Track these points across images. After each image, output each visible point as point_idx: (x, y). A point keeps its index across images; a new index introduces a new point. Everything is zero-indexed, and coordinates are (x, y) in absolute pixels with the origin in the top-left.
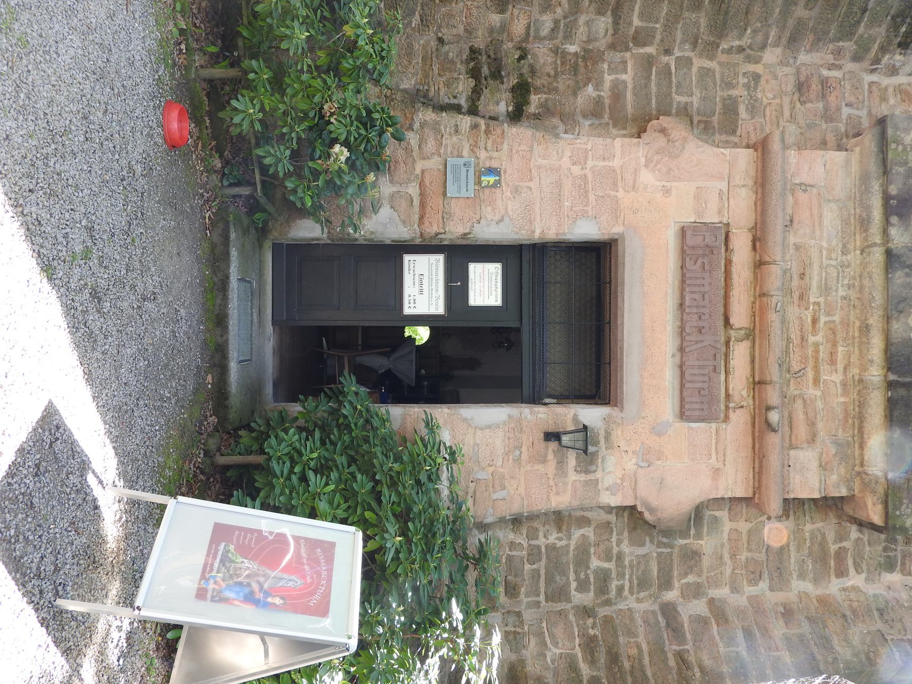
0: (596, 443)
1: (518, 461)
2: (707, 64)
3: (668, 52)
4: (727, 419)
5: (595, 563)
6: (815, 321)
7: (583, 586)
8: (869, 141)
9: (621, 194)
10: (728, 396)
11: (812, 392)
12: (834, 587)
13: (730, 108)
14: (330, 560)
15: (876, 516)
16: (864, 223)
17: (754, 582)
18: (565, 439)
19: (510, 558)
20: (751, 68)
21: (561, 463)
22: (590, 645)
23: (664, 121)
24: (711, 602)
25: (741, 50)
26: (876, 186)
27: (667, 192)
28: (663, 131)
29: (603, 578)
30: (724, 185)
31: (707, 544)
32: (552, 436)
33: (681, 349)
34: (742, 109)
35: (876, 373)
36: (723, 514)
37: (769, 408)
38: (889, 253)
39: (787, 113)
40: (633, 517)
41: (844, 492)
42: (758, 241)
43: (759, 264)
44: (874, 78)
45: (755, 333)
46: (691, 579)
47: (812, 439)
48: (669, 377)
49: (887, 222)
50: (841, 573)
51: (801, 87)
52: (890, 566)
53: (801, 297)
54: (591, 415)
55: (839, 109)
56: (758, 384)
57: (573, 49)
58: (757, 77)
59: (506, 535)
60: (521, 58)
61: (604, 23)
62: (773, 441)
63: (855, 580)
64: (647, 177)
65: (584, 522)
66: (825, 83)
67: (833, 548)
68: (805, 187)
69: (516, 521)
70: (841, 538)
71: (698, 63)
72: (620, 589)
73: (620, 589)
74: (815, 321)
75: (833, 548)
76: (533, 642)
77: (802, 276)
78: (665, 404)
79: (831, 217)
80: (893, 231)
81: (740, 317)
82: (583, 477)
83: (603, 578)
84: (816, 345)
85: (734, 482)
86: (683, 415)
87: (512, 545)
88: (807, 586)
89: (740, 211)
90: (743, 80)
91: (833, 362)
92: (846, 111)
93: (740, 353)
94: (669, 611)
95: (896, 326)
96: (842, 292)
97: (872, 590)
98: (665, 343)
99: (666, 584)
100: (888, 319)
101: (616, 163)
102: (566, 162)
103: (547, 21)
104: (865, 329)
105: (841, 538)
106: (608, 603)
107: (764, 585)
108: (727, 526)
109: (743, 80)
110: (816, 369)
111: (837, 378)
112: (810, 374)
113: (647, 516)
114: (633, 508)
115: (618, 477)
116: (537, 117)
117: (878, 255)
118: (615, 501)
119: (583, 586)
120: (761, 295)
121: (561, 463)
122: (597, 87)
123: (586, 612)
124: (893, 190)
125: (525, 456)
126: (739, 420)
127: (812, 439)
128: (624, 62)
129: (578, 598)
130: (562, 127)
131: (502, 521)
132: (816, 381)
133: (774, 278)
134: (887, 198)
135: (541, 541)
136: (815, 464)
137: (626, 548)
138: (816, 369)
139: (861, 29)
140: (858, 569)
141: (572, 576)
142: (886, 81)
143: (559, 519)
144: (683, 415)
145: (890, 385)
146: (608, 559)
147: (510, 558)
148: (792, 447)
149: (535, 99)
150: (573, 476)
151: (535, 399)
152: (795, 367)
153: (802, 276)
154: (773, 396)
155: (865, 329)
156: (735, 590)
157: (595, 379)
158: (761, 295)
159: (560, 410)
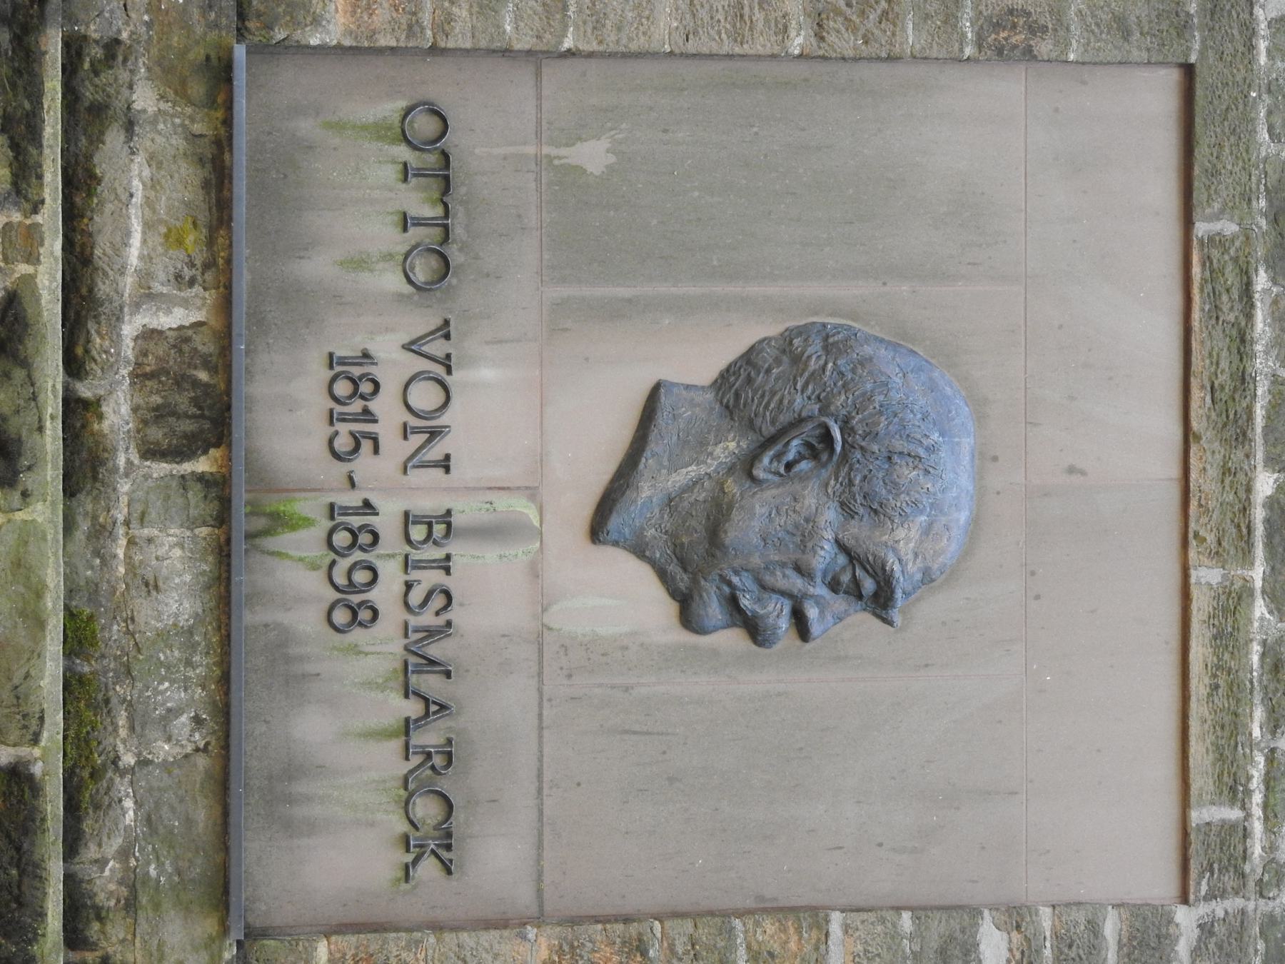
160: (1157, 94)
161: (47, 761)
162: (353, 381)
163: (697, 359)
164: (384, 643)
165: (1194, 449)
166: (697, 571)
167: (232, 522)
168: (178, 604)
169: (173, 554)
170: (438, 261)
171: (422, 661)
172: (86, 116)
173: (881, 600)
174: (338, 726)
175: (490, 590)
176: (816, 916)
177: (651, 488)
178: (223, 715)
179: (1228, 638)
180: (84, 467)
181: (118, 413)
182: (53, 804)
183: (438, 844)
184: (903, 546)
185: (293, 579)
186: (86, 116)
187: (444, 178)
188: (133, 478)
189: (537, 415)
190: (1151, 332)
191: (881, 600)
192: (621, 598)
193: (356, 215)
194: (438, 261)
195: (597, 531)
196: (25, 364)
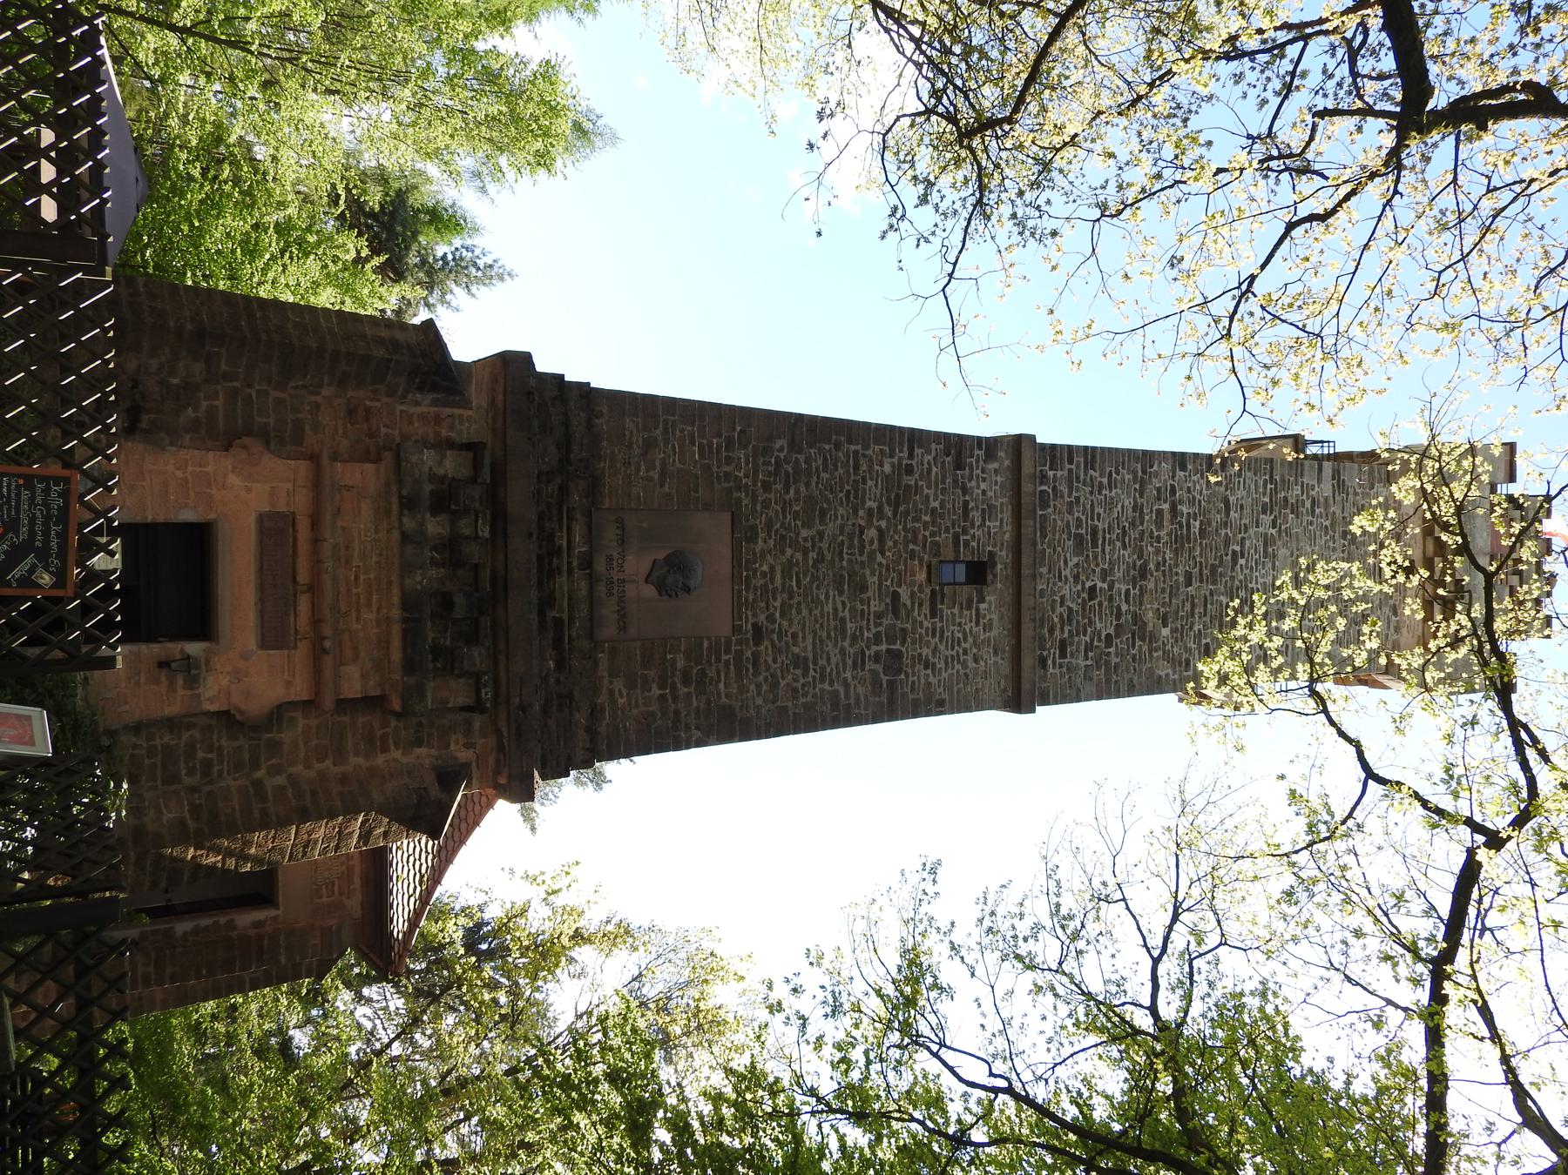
0: (198, 667)
1: (137, 683)
2: (282, 395)
3: (250, 386)
4: (296, 647)
5: (201, 755)
6: (357, 578)
7: (191, 772)
8: (388, 457)
9: (214, 491)
10: (296, 631)
11: (355, 626)
12: (380, 760)
13: (299, 427)
14: (31, 725)
15: (397, 707)
16: (388, 513)
17: (321, 760)
18: (174, 665)
19: (132, 756)
20: (313, 398)
21: (172, 683)
22: (196, 811)
23: (246, 440)
24: (290, 777)
25: (304, 387)
26: (394, 489)
27: (248, 490)
28: (245, 447)
29: (207, 765)
30: (290, 486)
31: (286, 736)
32: (163, 664)
33: (261, 600)
34: (307, 428)
35: (396, 613)
36: (298, 714)
37: (323, 638)
38: (403, 534)
39: (341, 432)
40: (228, 719)
41: (378, 693)
42: (315, 522)
43: (316, 541)
44: (403, 407)
45: (314, 588)
46: (274, 761)
47: (356, 658)
48: (252, 617)
49: (401, 515)
50: (385, 750)
51: (351, 413)
52: (419, 743)
53: (347, 562)
54: (194, 648)
55: (378, 429)
56: (316, 622)
57: (175, 381)
58: (318, 406)
59: (125, 739)
60: (134, 387)
61: (198, 368)
62: (328, 660)
63: (395, 754)
64: (233, 479)
65: (190, 726)
66: (368, 410)
67: (379, 733)
68: (348, 488)
69: (137, 728)
70: (384, 725)
71: (274, 394)
72: (220, 772)
73: (220, 772)
74: (357, 578)
75: (379, 733)
76: (152, 812)
77: (347, 548)
78: (251, 641)
79: (366, 509)
80: (405, 520)
81: (303, 577)
82: (189, 692)
83: (207, 765)
84: (358, 594)
85: (300, 690)
86: (264, 645)
87: (135, 746)
88: (360, 761)
89: (302, 502)
90: (307, 408)
91: (369, 605)
92: (384, 430)
93: (304, 603)
94: (258, 784)
95: (407, 581)
96: (375, 559)
97: (405, 760)
98: (249, 596)
99: (255, 766)
100: (402, 577)
101: (209, 469)
102: (171, 468)
103: (154, 364)
104: (390, 583)
105: (384, 725)
106: (211, 782)
107: (328, 762)
108: (301, 723)
109: (307, 408)
110: (358, 610)
111: (372, 616)
112: (354, 614)
113: (238, 717)
114: (228, 712)
115: (214, 691)
116: (147, 431)
117: (396, 535)
118: (213, 708)
119: (191, 772)
120: (317, 561)
121: (172, 683)
122: (196, 409)
123: (194, 789)
124: (404, 493)
125: (143, 680)
126: (304, 647)
127: (356, 658)
128: (217, 392)
129: (188, 781)
130: (167, 441)
131: (126, 727)
132: (358, 619)
133: (326, 549)
134: (401, 497)
135: (158, 742)
136: (357, 675)
137: (224, 743)
138: (358, 610)
139: (389, 378)
140: (397, 747)
141: (182, 765)
142: (412, 410)
143: (171, 724)
144: (264, 645)
145: (405, 620)
146: (211, 751)
147: (132, 756)
148: (342, 664)
149: (145, 418)
150: (181, 692)
151: (150, 639)
152: (344, 609)
153: (347, 548)
154: (327, 630)
155: (390, 583)
156: (308, 766)
157: (201, 624)
158: (317, 561)
159: (170, 645)
160: (727, 517)
161: (565, 616)
162: (610, 558)
163: (661, 555)
164: (615, 598)
165: (1287, 242)
166: (661, 587)
167: (592, 580)
168: (584, 593)
169: (583, 584)
170: (622, 541)
171: (621, 601)
172: (570, 519)
173: (688, 592)
174: (608, 611)
175: (631, 590)
176: (679, 639)
177: (655, 574)
178: (591, 609)
179: (740, 596)
180: (570, 572)
181: (575, 564)
182: (303, 527)
183: (623, 628)
184: (692, 583)
185: (601, 589)
186: (570, 519)
187: (623, 528)
188: (577, 573)
189: (637, 564)
190: (726, 551)
191: (688, 592)
192: (650, 591)
193: (610, 534)
194: (622, 541)
195: (646, 581)
196: (461, 393)
